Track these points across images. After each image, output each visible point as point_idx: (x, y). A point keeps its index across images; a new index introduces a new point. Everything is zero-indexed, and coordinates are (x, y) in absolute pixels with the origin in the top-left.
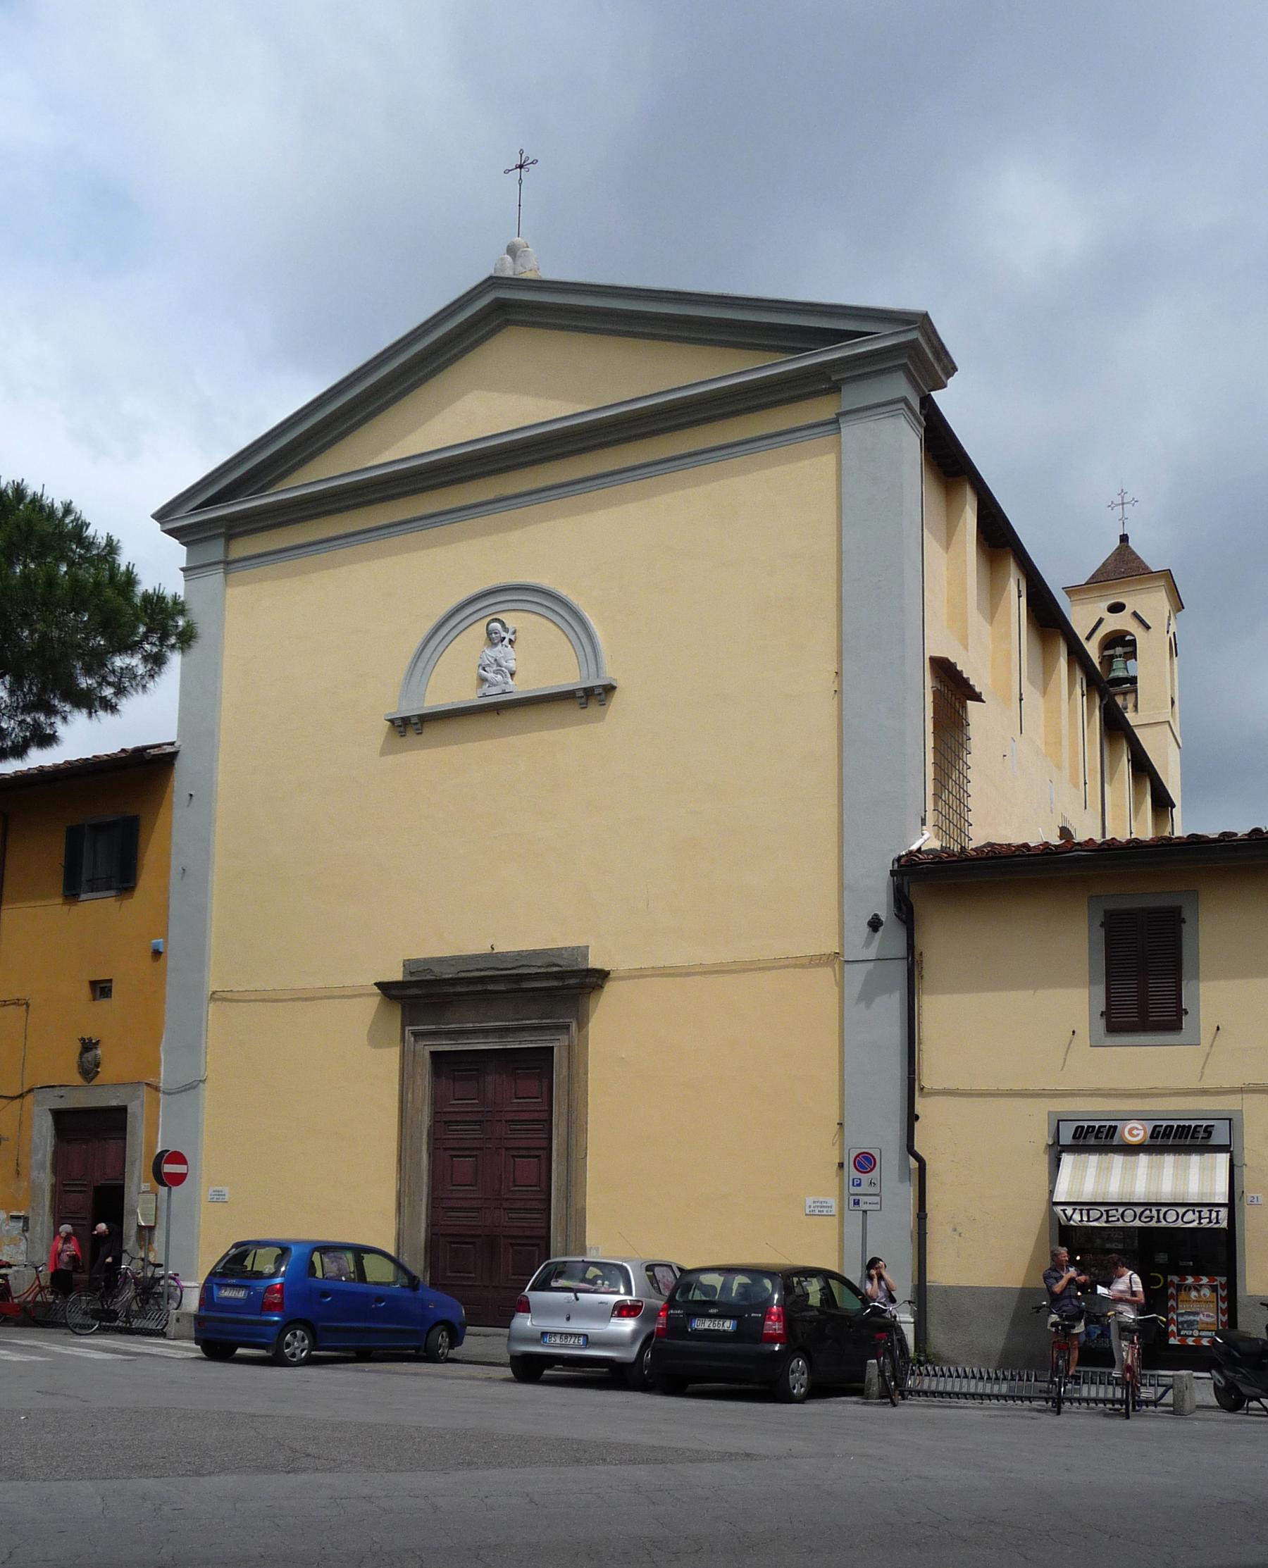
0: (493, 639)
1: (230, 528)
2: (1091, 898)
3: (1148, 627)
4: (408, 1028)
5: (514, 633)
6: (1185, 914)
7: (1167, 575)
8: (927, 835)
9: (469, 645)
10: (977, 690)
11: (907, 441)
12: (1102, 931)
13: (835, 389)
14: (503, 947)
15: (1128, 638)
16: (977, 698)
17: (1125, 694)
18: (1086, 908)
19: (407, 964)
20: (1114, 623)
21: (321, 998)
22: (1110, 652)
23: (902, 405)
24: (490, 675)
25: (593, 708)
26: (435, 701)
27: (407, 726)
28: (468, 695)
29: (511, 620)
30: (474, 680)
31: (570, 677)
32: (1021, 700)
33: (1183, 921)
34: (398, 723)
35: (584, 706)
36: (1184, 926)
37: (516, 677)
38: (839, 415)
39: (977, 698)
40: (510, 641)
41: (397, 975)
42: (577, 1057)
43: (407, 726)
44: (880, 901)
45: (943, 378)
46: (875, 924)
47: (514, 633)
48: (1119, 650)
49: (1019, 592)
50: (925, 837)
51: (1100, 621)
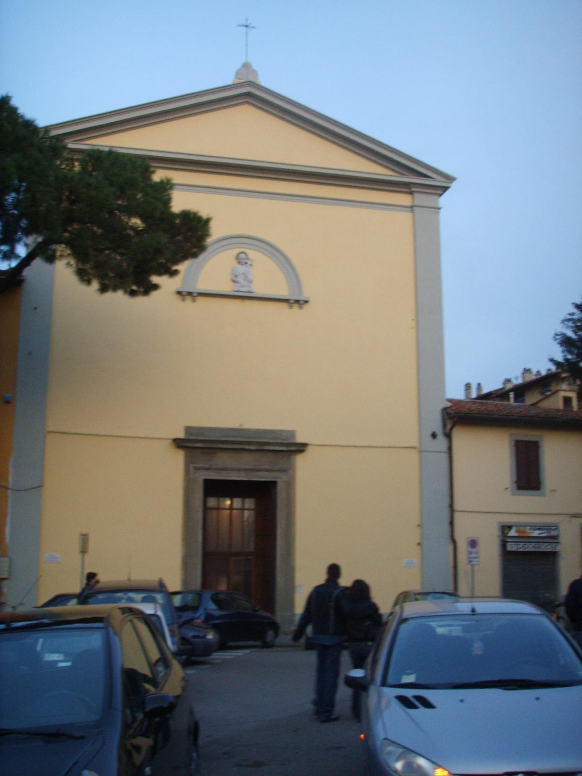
4: (192, 465)
14: (247, 426)
19: (188, 429)
21: (439, 593)
28: (227, 287)
41: (181, 435)
42: (290, 485)
44: (436, 423)
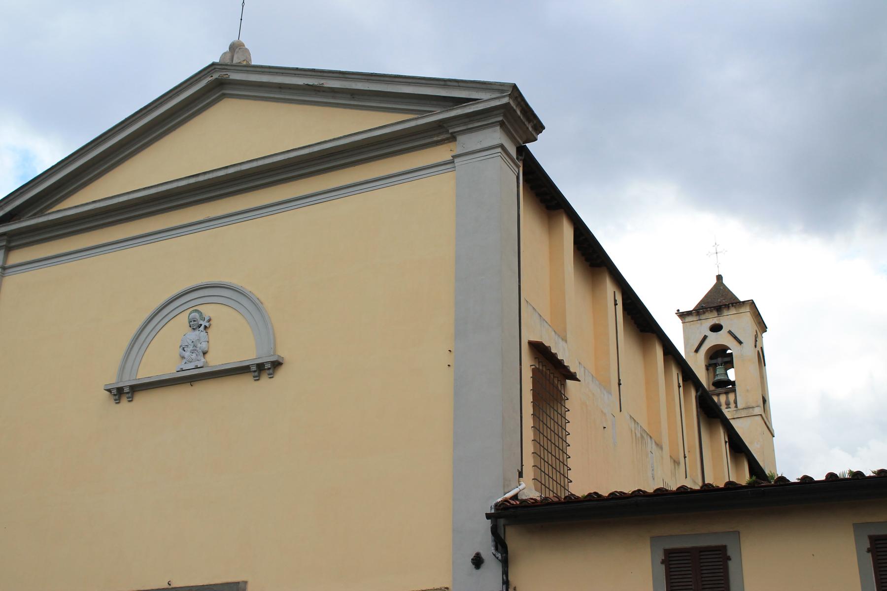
0: (195, 325)
1: (9, 242)
2: (652, 538)
3: (740, 343)
5: (209, 320)
6: (730, 553)
7: (752, 304)
8: (523, 485)
9: (177, 329)
10: (572, 370)
11: (504, 177)
12: (663, 567)
13: (453, 138)
15: (729, 351)
16: (573, 377)
17: (727, 393)
18: (649, 550)
20: (714, 339)
22: (714, 361)
23: (499, 150)
24: (187, 354)
25: (265, 380)
26: (146, 372)
27: (119, 393)
28: (168, 368)
29: (208, 311)
30: (178, 356)
31: (249, 355)
32: (620, 384)
33: (729, 558)
34: (115, 392)
35: (257, 378)
36: (730, 563)
37: (207, 356)
38: (454, 157)
39: (573, 377)
40: (206, 327)
43: (119, 393)
45: (534, 133)
46: (478, 561)
47: (209, 320)
48: (719, 360)
49: (615, 301)
50: (521, 487)
51: (705, 337)
